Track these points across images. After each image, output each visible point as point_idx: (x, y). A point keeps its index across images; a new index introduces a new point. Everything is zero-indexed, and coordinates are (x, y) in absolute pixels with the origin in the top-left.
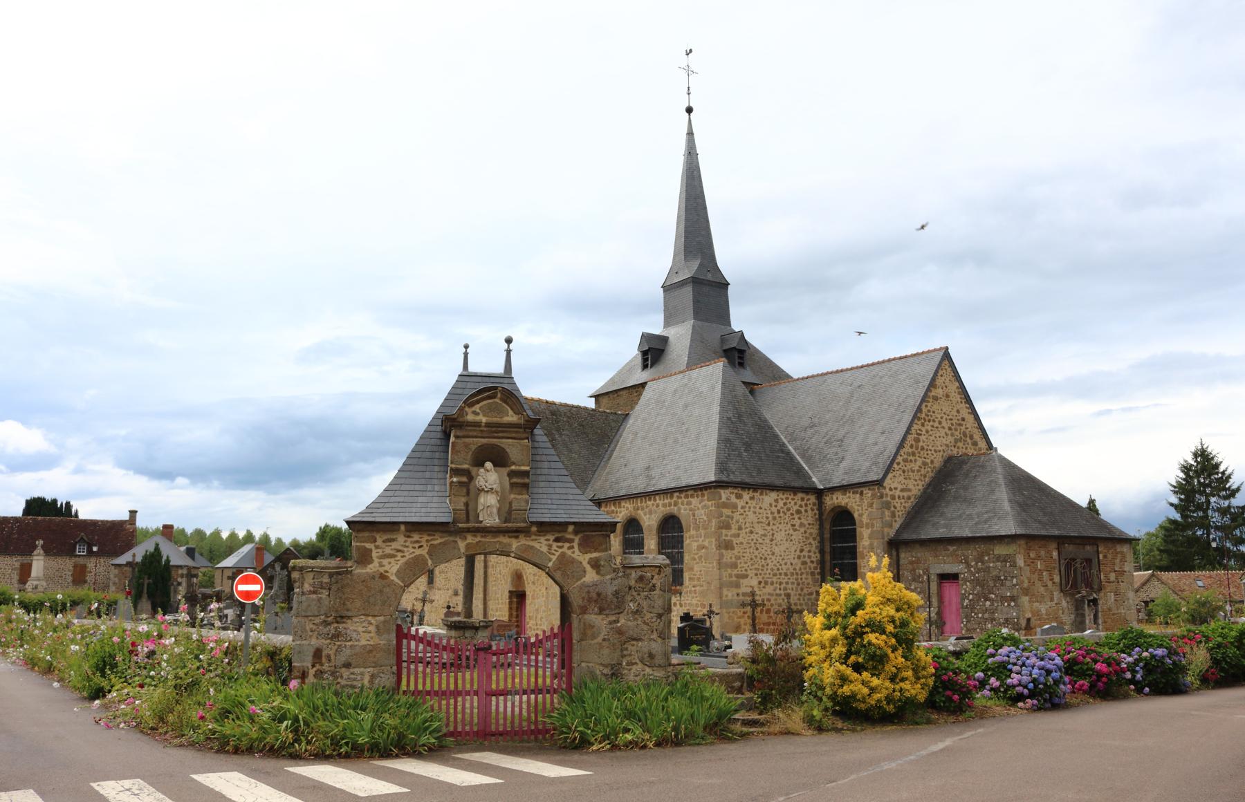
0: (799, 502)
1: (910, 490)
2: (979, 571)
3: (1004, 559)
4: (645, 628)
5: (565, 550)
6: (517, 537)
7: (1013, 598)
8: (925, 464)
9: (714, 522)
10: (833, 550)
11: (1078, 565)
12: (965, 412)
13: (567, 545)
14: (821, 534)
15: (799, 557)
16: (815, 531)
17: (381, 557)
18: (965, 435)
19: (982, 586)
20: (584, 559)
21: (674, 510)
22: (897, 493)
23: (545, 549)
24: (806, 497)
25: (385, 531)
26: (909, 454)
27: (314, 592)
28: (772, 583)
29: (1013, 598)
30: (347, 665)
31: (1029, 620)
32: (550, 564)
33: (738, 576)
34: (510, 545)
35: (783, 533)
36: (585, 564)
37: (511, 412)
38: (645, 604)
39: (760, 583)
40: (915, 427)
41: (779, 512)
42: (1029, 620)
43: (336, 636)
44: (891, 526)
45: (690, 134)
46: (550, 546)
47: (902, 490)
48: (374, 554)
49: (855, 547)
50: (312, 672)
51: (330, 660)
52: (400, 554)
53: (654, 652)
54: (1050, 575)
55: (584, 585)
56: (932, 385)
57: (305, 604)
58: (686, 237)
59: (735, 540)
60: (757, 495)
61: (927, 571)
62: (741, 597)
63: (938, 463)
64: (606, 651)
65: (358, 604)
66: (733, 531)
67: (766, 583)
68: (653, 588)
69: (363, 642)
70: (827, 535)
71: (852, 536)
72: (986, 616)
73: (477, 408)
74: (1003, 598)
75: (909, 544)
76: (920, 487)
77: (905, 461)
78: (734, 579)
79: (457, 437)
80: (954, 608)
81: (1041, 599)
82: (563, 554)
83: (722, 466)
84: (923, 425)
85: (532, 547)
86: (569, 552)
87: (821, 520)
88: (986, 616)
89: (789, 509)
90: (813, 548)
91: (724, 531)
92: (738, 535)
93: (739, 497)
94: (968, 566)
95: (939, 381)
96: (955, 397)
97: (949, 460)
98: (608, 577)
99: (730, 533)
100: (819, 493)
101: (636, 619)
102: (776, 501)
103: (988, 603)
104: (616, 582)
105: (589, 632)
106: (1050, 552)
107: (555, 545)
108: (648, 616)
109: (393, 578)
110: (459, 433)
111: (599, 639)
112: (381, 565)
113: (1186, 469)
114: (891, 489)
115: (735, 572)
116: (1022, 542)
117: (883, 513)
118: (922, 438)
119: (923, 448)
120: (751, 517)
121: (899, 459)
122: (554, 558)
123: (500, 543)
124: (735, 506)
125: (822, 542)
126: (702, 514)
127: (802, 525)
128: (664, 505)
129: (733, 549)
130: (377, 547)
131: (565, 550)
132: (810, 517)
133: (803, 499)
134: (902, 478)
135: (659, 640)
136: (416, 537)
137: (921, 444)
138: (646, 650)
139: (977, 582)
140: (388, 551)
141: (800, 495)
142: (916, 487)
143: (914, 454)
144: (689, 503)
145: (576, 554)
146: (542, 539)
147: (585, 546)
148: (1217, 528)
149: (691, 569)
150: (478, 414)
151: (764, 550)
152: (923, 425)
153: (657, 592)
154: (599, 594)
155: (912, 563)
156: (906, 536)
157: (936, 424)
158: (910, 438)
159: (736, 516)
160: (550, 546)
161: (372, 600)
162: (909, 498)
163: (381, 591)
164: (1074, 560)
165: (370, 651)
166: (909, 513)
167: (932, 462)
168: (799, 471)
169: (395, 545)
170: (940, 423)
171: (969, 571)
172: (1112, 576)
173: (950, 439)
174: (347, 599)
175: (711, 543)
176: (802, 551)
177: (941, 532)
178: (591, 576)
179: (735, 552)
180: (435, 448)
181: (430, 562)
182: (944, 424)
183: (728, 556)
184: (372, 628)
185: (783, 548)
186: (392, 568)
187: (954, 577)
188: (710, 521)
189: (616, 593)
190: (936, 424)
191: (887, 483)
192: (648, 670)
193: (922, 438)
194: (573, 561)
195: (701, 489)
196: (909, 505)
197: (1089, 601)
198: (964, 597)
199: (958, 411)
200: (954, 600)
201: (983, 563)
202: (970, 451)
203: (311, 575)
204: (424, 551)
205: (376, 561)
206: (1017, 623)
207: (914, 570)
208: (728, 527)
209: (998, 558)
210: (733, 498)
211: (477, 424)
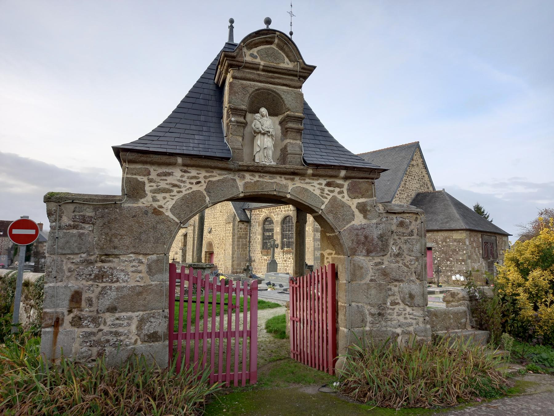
2: (444, 246)
3: (459, 241)
4: (406, 269)
5: (335, 194)
6: (293, 180)
7: (463, 260)
8: (408, 196)
12: (424, 173)
13: (337, 190)
17: (154, 192)
18: (424, 184)
19: (446, 254)
20: (353, 203)
23: (317, 192)
25: (160, 164)
26: (402, 190)
27: (75, 227)
29: (463, 260)
30: (112, 309)
32: (323, 207)
34: (286, 187)
36: (354, 207)
37: (287, 60)
38: (404, 247)
40: (405, 178)
43: (100, 277)
46: (322, 190)
48: (147, 188)
50: (68, 318)
51: (91, 305)
52: (175, 189)
53: (413, 293)
54: (479, 250)
55: (353, 228)
57: (62, 241)
63: (413, 196)
64: (373, 292)
65: (127, 241)
68: (411, 234)
69: (132, 284)
72: (448, 268)
73: (255, 51)
74: (458, 260)
77: (400, 193)
79: (234, 78)
81: (474, 261)
82: (334, 199)
85: (307, 190)
86: (339, 197)
88: (448, 268)
95: (415, 158)
96: (421, 166)
97: (418, 195)
98: (374, 221)
101: (397, 262)
103: (449, 262)
104: (381, 226)
105: (358, 273)
106: (478, 238)
107: (327, 189)
108: (408, 258)
109: (169, 214)
110: (237, 74)
111: (367, 280)
112: (155, 200)
116: (468, 233)
119: (407, 188)
121: (398, 193)
122: (326, 201)
123: (277, 184)
128: (285, 211)
130: (151, 181)
131: (335, 194)
135: (418, 282)
136: (193, 172)
137: (407, 186)
138: (406, 291)
140: (163, 185)
143: (404, 191)
145: (346, 198)
146: (315, 183)
147: (354, 192)
150: (255, 57)
153: (415, 237)
154: (366, 237)
157: (413, 178)
160: (322, 190)
161: (143, 237)
163: (154, 228)
165: (140, 293)
167: (411, 195)
169: (170, 179)
174: (115, 235)
178: (359, 220)
180: (208, 97)
181: (208, 199)
182: (416, 178)
184: (143, 268)
186: (167, 203)
189: (381, 237)
190: (413, 178)
192: (409, 309)
193: (407, 183)
194: (343, 205)
201: (446, 242)
202: (426, 190)
203: (71, 207)
204: (202, 188)
205: (150, 195)
209: (455, 240)
211: (254, 67)
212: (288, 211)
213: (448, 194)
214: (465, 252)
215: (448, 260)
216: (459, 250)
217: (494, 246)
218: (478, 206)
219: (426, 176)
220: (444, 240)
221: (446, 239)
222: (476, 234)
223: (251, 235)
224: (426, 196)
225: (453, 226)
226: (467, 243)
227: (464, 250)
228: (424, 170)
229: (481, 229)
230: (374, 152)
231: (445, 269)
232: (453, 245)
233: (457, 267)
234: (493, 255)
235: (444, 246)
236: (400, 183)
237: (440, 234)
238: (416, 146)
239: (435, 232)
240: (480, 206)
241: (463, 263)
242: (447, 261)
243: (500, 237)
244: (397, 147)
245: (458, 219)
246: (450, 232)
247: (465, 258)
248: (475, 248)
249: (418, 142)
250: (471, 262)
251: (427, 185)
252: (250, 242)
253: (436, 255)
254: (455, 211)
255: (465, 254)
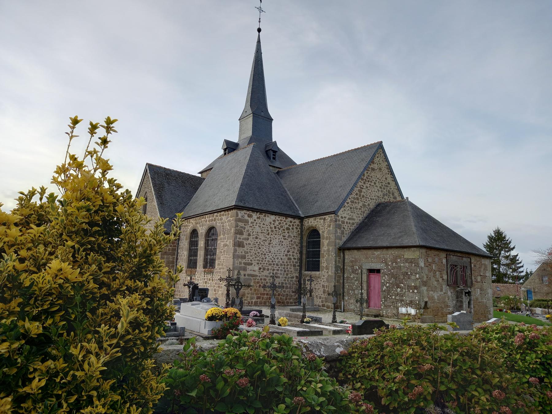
0: (289, 223)
1: (354, 219)
2: (393, 268)
3: (411, 261)
7: (415, 287)
8: (364, 205)
9: (233, 230)
10: (308, 252)
11: (458, 269)
12: (390, 180)
14: (301, 243)
15: (286, 255)
16: (297, 241)
18: (389, 192)
19: (396, 278)
21: (213, 223)
22: (346, 220)
24: (293, 221)
26: (354, 198)
28: (268, 270)
29: (415, 287)
31: (426, 303)
33: (245, 264)
35: (277, 240)
39: (260, 269)
40: (360, 183)
41: (275, 228)
42: (426, 303)
44: (341, 239)
45: (259, 42)
47: (349, 219)
49: (319, 251)
56: (372, 161)
58: (252, 94)
59: (245, 242)
60: (262, 216)
61: (361, 267)
62: (247, 277)
63: (372, 206)
66: (244, 236)
67: (264, 269)
70: (305, 244)
71: (318, 244)
72: (398, 298)
74: (409, 287)
75: (349, 249)
76: (361, 218)
77: (352, 202)
78: (243, 265)
80: (377, 291)
81: (434, 289)
83: (240, 197)
84: (364, 183)
87: (301, 235)
88: (398, 298)
89: (282, 227)
90: (296, 251)
91: (238, 236)
92: (248, 239)
93: (250, 216)
94: (387, 265)
95: (376, 160)
97: (379, 205)
99: (242, 237)
100: (301, 219)
102: (274, 221)
103: (399, 290)
113: (490, 238)
114: (342, 217)
115: (244, 261)
116: (424, 251)
117: (336, 231)
118: (363, 190)
119: (363, 196)
120: (257, 229)
121: (349, 201)
124: (247, 222)
125: (301, 247)
126: (227, 225)
127: (289, 236)
128: (209, 221)
129: (243, 247)
132: (295, 233)
133: (291, 222)
134: (349, 212)
137: (362, 194)
139: (393, 275)
141: (290, 219)
142: (358, 218)
143: (358, 199)
144: (221, 219)
148: (503, 265)
149: (219, 258)
151: (264, 249)
152: (364, 183)
155: (352, 262)
156: (349, 245)
157: (373, 184)
158: (356, 190)
159: (247, 227)
162: (353, 224)
164: (456, 266)
166: (353, 232)
167: (369, 205)
168: (291, 206)
170: (375, 183)
171: (387, 268)
172: (479, 279)
173: (380, 194)
175: (230, 242)
176: (288, 252)
177: (371, 244)
179: (245, 249)
182: (377, 184)
183: (240, 251)
185: (276, 249)
187: (378, 271)
188: (231, 229)
191: (340, 213)
193: (363, 190)
195: (228, 210)
196: (353, 228)
197: (466, 293)
198: (383, 284)
199: (386, 179)
200: (377, 286)
201: (396, 263)
202: (392, 200)
206: (419, 304)
207: (353, 266)
208: (241, 233)
209: (407, 260)
210: (246, 217)
212: (212, 220)
213: (412, 205)
214: (417, 276)
215: (398, 287)
216: (411, 274)
217: (468, 273)
218: (499, 231)
219: (393, 184)
220: (394, 261)
221: (396, 259)
222: (437, 253)
223: (179, 251)
224: (387, 206)
225: (406, 242)
226: (422, 264)
227: (416, 273)
228: (389, 176)
229: (446, 248)
230: (334, 155)
231: (395, 299)
232: (404, 267)
233: (409, 296)
234: (465, 283)
235: (393, 268)
236: (352, 189)
237: (391, 252)
238: (379, 146)
239: (384, 250)
240: (501, 230)
241: (416, 291)
242: (397, 288)
243: (478, 259)
244: (358, 149)
245: (414, 233)
246: (401, 250)
247: (418, 285)
248: (435, 272)
249: (381, 142)
250: (427, 290)
251: (393, 194)
252: (177, 259)
253: (384, 280)
254: (413, 224)
255: (417, 279)
